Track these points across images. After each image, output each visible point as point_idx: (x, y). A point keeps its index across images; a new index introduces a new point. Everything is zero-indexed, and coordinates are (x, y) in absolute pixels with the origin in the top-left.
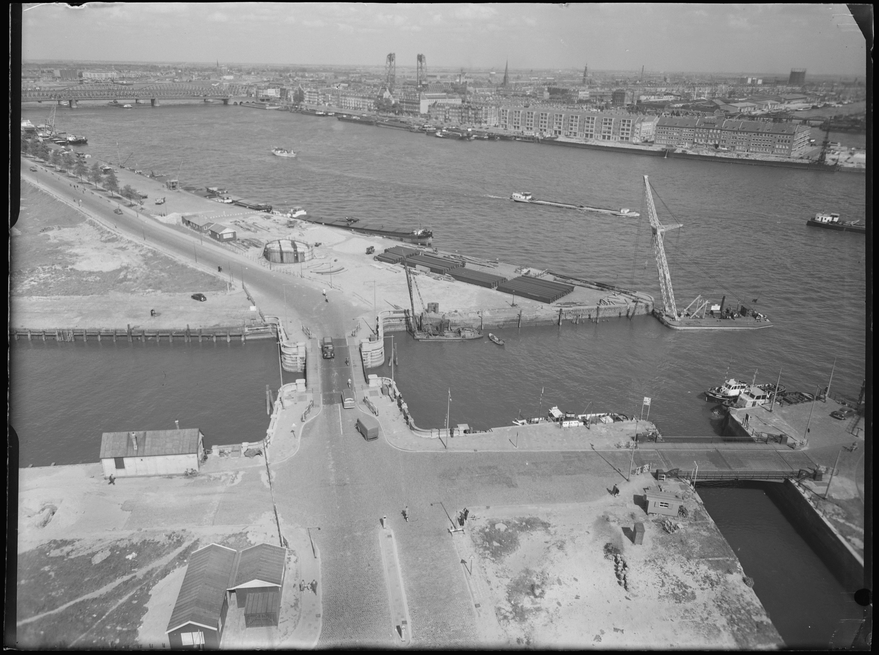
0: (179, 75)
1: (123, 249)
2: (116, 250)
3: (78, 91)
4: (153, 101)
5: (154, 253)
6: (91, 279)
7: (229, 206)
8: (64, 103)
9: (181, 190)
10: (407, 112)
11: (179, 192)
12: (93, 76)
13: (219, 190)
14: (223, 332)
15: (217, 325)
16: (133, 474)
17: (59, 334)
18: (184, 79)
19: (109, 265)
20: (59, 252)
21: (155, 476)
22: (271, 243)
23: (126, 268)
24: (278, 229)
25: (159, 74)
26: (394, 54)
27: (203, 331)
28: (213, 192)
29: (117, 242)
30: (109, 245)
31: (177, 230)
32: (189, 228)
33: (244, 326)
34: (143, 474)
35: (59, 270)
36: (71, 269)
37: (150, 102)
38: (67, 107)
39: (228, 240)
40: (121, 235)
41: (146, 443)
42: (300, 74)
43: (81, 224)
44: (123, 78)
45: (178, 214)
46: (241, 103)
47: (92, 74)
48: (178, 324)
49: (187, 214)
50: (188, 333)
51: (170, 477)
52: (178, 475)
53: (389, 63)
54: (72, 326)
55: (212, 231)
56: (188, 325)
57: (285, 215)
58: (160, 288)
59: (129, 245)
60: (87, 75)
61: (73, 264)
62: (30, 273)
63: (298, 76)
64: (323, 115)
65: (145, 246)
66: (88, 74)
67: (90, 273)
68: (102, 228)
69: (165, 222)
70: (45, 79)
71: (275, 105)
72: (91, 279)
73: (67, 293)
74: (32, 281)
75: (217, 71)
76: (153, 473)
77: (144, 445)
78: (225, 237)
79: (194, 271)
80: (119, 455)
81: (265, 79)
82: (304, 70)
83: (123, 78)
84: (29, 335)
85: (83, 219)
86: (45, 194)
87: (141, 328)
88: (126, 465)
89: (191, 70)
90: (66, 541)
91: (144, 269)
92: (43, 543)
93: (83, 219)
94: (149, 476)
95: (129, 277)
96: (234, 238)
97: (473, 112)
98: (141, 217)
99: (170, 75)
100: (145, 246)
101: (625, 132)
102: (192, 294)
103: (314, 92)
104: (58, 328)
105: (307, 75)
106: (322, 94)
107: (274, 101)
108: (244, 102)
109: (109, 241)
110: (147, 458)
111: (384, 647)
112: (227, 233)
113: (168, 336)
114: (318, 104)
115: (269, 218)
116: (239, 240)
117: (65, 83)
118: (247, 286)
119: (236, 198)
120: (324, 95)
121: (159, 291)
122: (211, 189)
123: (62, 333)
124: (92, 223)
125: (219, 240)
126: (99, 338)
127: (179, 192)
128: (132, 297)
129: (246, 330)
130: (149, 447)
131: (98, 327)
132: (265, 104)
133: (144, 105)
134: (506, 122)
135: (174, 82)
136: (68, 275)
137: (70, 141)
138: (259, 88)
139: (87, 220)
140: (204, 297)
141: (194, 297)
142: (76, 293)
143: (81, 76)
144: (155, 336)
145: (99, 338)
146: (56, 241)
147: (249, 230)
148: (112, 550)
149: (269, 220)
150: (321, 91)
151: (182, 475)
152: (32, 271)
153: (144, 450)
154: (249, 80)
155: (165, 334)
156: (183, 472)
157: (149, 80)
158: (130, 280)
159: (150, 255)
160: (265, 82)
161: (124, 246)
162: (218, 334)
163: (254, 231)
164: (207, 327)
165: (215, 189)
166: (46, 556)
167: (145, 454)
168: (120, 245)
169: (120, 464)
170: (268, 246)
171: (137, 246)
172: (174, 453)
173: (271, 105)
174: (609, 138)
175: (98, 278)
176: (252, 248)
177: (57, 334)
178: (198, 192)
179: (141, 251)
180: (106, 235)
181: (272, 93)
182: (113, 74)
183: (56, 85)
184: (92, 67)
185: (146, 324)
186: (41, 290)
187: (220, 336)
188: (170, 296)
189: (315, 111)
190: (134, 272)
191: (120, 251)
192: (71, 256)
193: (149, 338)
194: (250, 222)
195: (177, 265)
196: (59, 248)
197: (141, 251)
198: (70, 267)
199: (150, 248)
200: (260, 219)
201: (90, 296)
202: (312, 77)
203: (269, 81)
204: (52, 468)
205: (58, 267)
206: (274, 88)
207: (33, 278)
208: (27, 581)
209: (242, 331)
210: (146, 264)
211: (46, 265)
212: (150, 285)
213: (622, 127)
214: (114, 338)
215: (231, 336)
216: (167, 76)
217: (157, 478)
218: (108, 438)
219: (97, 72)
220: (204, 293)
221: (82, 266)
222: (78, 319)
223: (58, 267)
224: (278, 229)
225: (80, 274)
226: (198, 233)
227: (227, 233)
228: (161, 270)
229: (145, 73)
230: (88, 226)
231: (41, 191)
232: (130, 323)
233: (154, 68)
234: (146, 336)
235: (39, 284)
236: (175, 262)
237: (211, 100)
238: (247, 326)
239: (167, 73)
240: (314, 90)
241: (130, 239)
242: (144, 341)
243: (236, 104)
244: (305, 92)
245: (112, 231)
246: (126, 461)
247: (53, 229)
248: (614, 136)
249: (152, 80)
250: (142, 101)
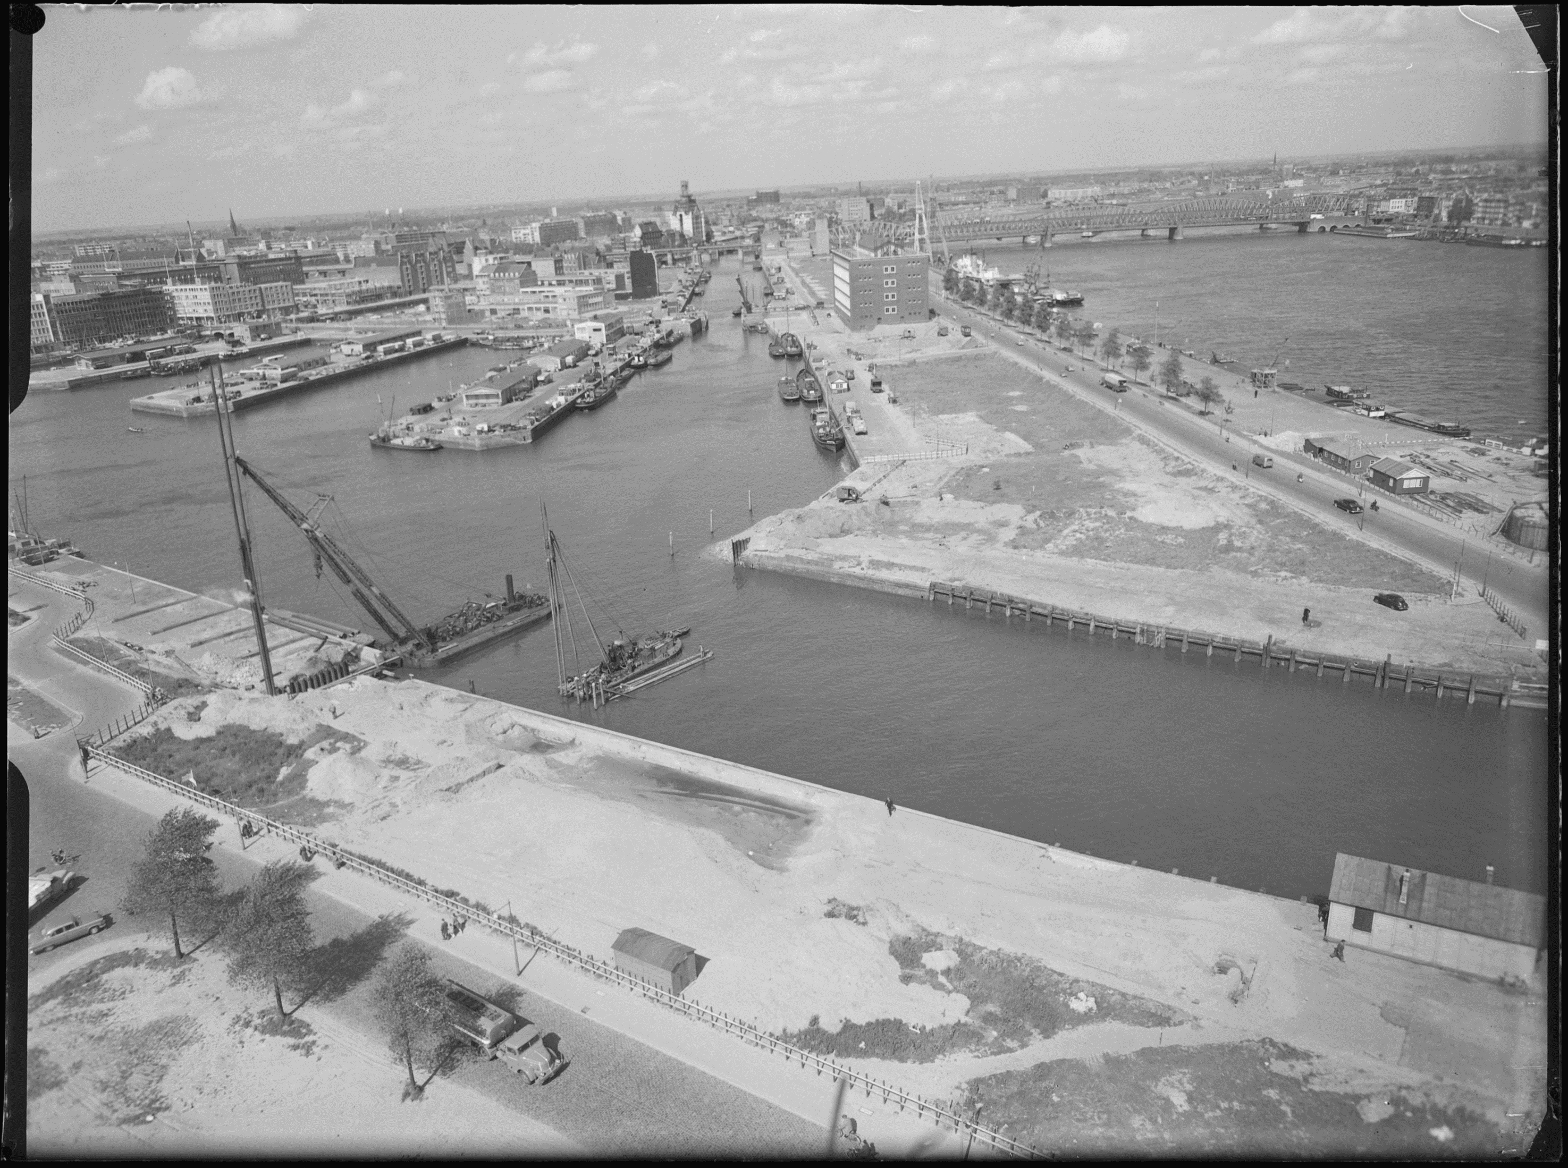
0: (1206, 185)
1: (1211, 491)
2: (1197, 492)
4: (1173, 231)
5: (1272, 503)
6: (1169, 538)
7: (1379, 422)
8: (1032, 240)
9: (1277, 389)
11: (1274, 392)
12: (1063, 195)
13: (1353, 391)
14: (1461, 682)
15: (1445, 665)
16: (1386, 947)
17: (1142, 631)
18: (1213, 191)
19: (1195, 518)
20: (1102, 486)
21: (1429, 965)
22: (1522, 506)
23: (1227, 526)
24: (1513, 478)
25: (1168, 185)
27: (1416, 672)
28: (1340, 394)
29: (1195, 478)
30: (1183, 481)
31: (1295, 461)
32: (1319, 460)
33: (1511, 677)
34: (1405, 955)
35: (1112, 517)
36: (1131, 518)
37: (1166, 233)
38: (1035, 245)
39: (1411, 492)
40: (1202, 466)
41: (1426, 896)
42: (1440, 167)
43: (1124, 441)
44: (1113, 196)
45: (1297, 434)
46: (1333, 228)
47: (1063, 191)
48: (1340, 646)
49: (1313, 435)
50: (1385, 670)
51: (1464, 977)
52: (1482, 979)
54: (1161, 621)
55: (1375, 471)
56: (1389, 656)
57: (1515, 450)
58: (1303, 573)
59: (1219, 484)
60: (1055, 193)
61: (1134, 510)
62: (1067, 518)
63: (1435, 172)
64: (1519, 246)
65: (1252, 490)
66: (1057, 191)
67: (1164, 529)
68: (1163, 450)
69: (1273, 447)
70: (994, 203)
71: (1405, 230)
72: (1169, 538)
73: (1135, 560)
74: (1076, 531)
75: (1270, 172)
76: (1428, 959)
77: (1421, 900)
78: (1406, 485)
79: (1359, 547)
80: (1367, 904)
81: (1378, 182)
82: (1448, 160)
83: (1113, 196)
84: (1092, 625)
85: (1127, 432)
86: (1055, 386)
87: (1289, 645)
88: (1374, 927)
89: (1222, 173)
90: (1294, 1050)
91: (1259, 532)
92: (1248, 1036)
93: (1127, 432)
94: (1416, 962)
95: (1237, 544)
96: (1423, 490)
98: (1233, 438)
99: (1187, 185)
100: (1252, 490)
102: (1377, 592)
103: (1499, 201)
104: (1141, 621)
105: (1454, 169)
106: (1516, 204)
107: (1401, 222)
108: (1340, 226)
109: (1180, 473)
111: (776, 1153)
112: (1412, 478)
113: (1343, 670)
114: (1505, 224)
115: (1482, 453)
116: (1432, 492)
117: (1024, 208)
118: (1490, 592)
119: (1390, 410)
120: (1522, 204)
121: (1304, 580)
122: (1336, 388)
123: (1147, 631)
124: (1143, 440)
125: (1392, 490)
126: (1210, 651)
127: (1274, 392)
128: (1256, 583)
129: (1516, 686)
130: (1432, 905)
131: (1209, 630)
132: (1383, 229)
133: (1155, 238)
135: (1195, 196)
136: (1128, 528)
137: (1058, 301)
138: (1370, 199)
139: (1134, 435)
140: (1403, 602)
141: (1380, 599)
142: (1152, 561)
143: (1045, 195)
144: (1317, 665)
145: (1210, 651)
146: (1092, 467)
147: (1448, 475)
148: (1395, 1101)
149: (1482, 458)
150: (1516, 197)
151: (1492, 982)
152: (1071, 514)
153: (1420, 908)
154: (1340, 186)
155: (1336, 665)
156: (1494, 976)
157: (1152, 196)
158: (1240, 549)
159: (1263, 506)
160: (1377, 186)
161: (1210, 486)
162: (1448, 684)
163: (1461, 479)
164: (1427, 666)
165: (1345, 389)
166: (1266, 1068)
167: (1423, 918)
168: (1202, 483)
169: (1363, 921)
170: (1518, 513)
171: (1234, 488)
172: (1488, 932)
173: (1398, 230)
175: (1181, 540)
176: (1468, 514)
177: (1138, 630)
178: (1310, 394)
179: (1243, 497)
180: (1173, 463)
181: (1397, 206)
182: (1096, 190)
183: (1010, 211)
184: (1057, 180)
185: (1296, 639)
186: (1094, 548)
187: (1452, 689)
188: (1330, 590)
189: (1502, 238)
190: (1243, 536)
191: (1204, 493)
192: (1126, 495)
193: (1302, 667)
194: (1444, 459)
195: (1322, 532)
196: (1101, 479)
197: (1243, 497)
198: (1129, 514)
199: (1261, 493)
200: (1458, 451)
201: (1179, 570)
202: (1466, 172)
203: (1385, 185)
204: (1211, 886)
205: (1111, 513)
206: (1405, 196)
207: (1076, 527)
208: (1244, 1107)
209: (1506, 688)
210: (1260, 522)
211: (1090, 506)
212: (1283, 565)
214: (1238, 654)
215: (1476, 692)
216: (1182, 187)
217: (1433, 970)
218: (1346, 866)
219: (1070, 187)
220: (1406, 596)
221: (1146, 514)
222: (1170, 610)
223: (1111, 513)
224: (1513, 478)
225: (1146, 527)
226: (1343, 472)
227: (1412, 478)
228: (1293, 537)
229: (1145, 185)
230: (1136, 445)
231: (1048, 382)
232: (1272, 633)
233: (1154, 175)
234: (1297, 662)
235: (1088, 537)
236: (1317, 525)
237: (1273, 226)
238: (1522, 679)
239: (1182, 183)
240: (1499, 196)
241: (1220, 473)
242: (1292, 669)
243: (1323, 230)
244: (1475, 201)
245: (1184, 457)
246: (1379, 920)
247: (1082, 446)
249: (1158, 195)
250: (1151, 233)
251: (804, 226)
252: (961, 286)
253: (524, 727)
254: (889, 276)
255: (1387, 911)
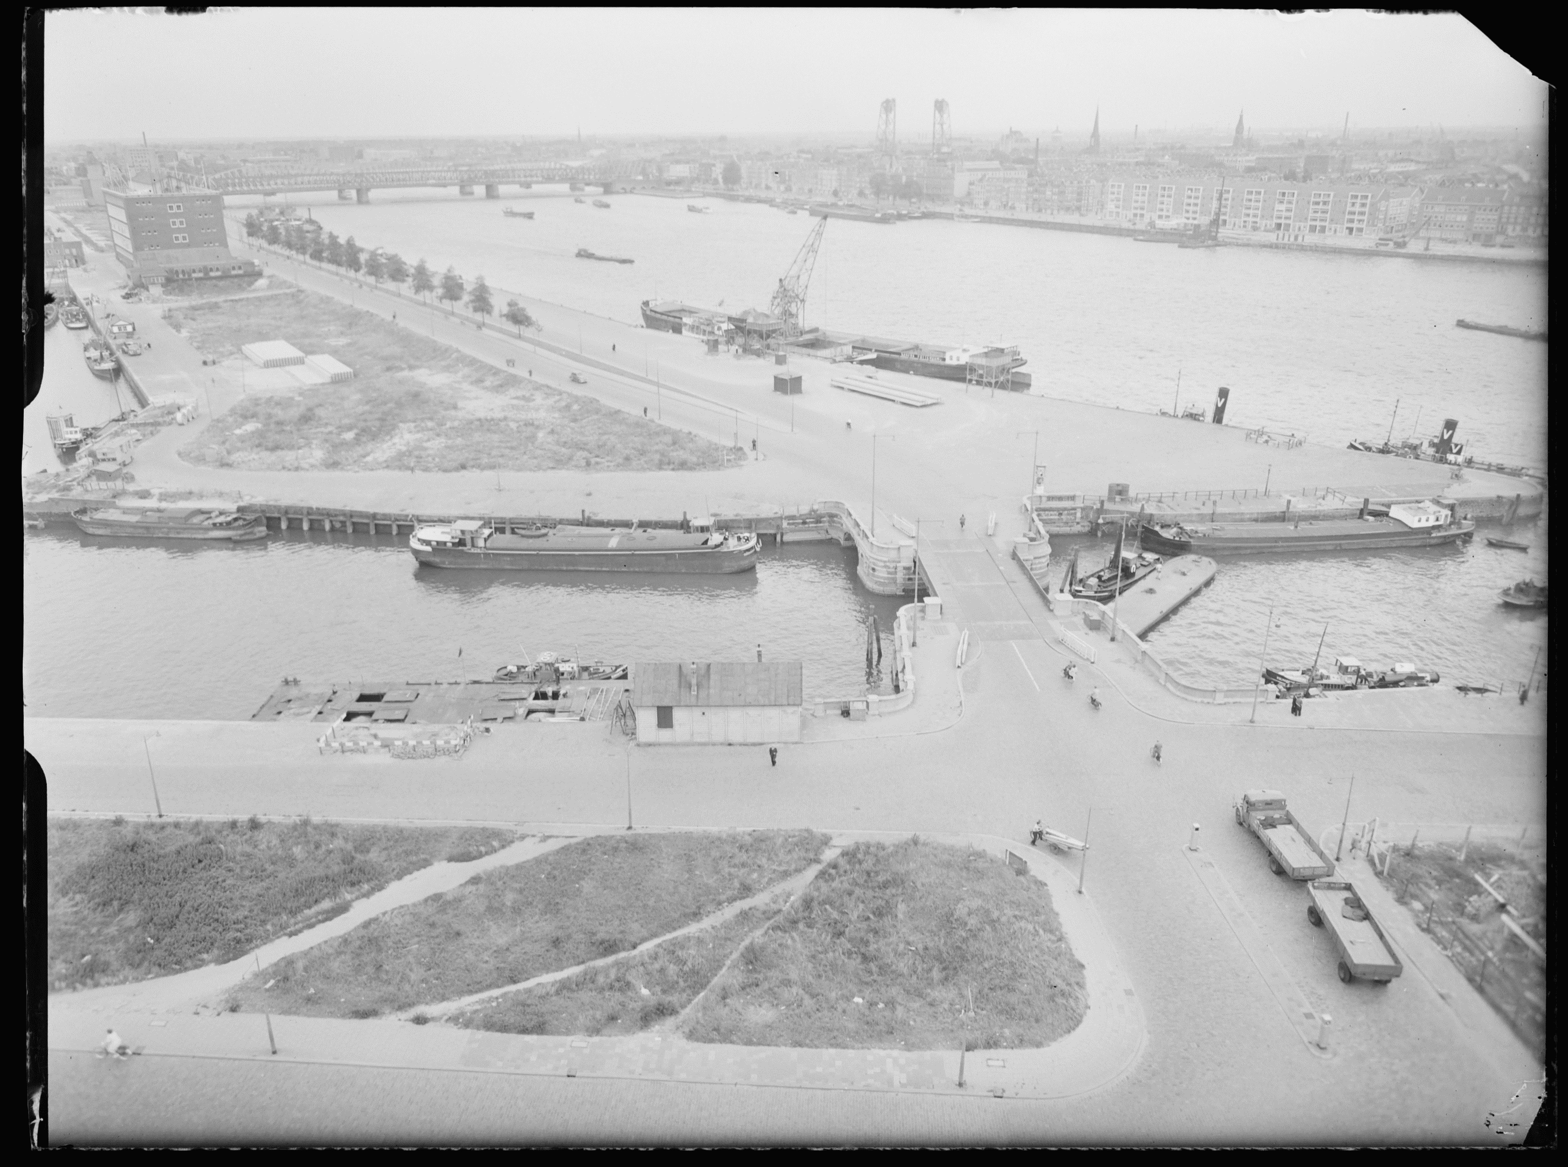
3: (186, 246)
10: (928, 195)
26: (894, 100)
53: (884, 116)
60: (370, 153)
80: (666, 703)
88: (675, 722)
97: (1056, 190)
101: (1356, 217)
110: (713, 710)
134: (1117, 207)
151: (328, 384)
153: (708, 695)
169: (665, 717)
172: (762, 703)
174: (1323, 229)
184: (371, 143)
213: (1349, 208)
246: (678, 715)
248: (1333, 226)
251: (73, 173)
252: (265, 228)
253: (569, 394)
254: (176, 215)
255: (682, 704)
